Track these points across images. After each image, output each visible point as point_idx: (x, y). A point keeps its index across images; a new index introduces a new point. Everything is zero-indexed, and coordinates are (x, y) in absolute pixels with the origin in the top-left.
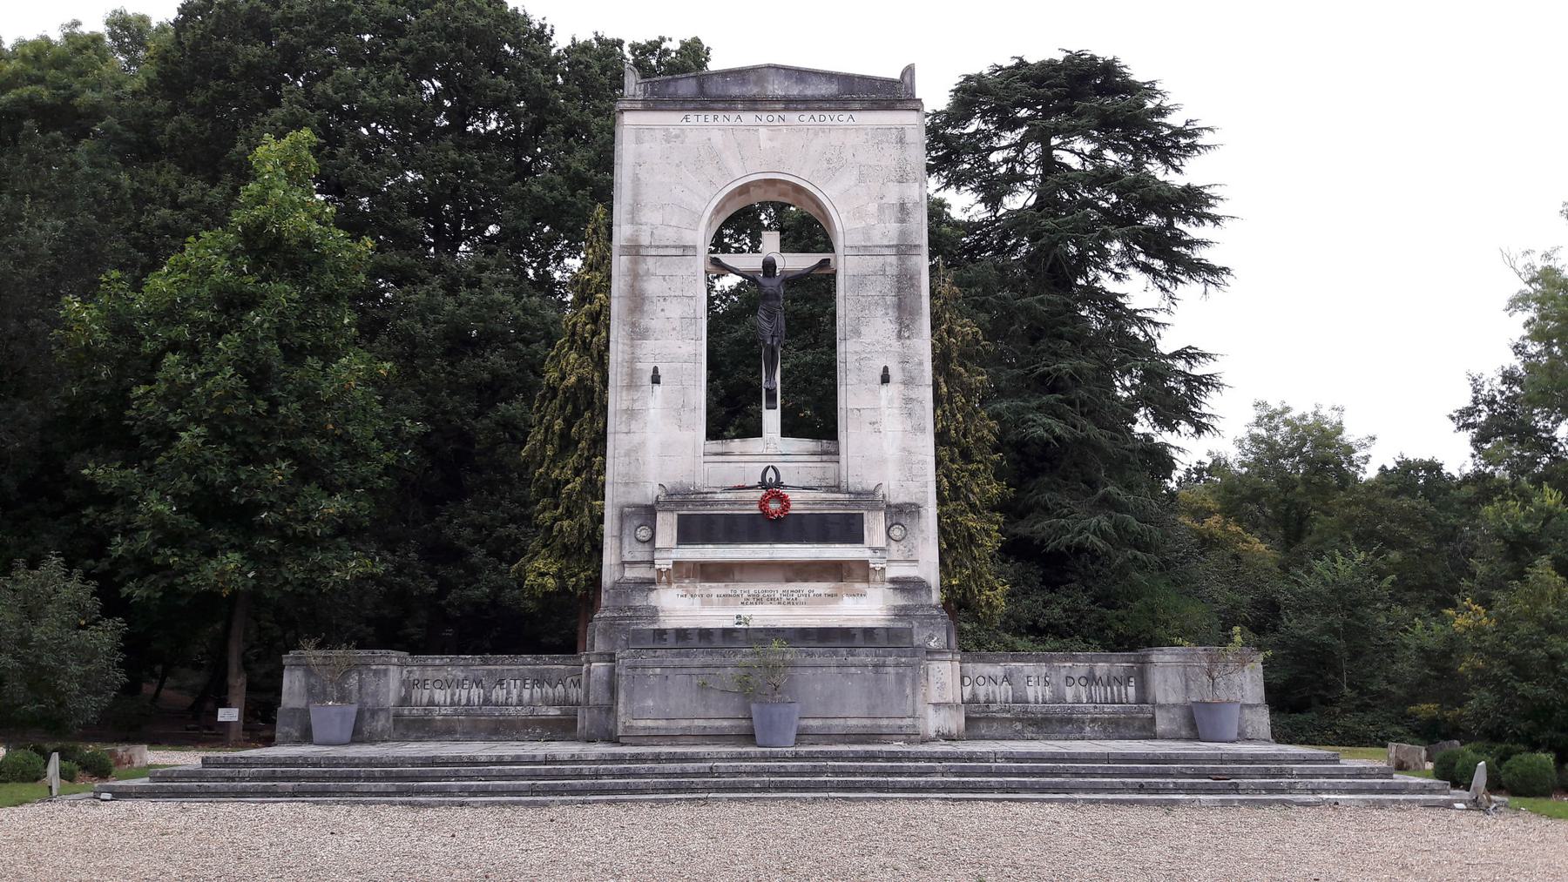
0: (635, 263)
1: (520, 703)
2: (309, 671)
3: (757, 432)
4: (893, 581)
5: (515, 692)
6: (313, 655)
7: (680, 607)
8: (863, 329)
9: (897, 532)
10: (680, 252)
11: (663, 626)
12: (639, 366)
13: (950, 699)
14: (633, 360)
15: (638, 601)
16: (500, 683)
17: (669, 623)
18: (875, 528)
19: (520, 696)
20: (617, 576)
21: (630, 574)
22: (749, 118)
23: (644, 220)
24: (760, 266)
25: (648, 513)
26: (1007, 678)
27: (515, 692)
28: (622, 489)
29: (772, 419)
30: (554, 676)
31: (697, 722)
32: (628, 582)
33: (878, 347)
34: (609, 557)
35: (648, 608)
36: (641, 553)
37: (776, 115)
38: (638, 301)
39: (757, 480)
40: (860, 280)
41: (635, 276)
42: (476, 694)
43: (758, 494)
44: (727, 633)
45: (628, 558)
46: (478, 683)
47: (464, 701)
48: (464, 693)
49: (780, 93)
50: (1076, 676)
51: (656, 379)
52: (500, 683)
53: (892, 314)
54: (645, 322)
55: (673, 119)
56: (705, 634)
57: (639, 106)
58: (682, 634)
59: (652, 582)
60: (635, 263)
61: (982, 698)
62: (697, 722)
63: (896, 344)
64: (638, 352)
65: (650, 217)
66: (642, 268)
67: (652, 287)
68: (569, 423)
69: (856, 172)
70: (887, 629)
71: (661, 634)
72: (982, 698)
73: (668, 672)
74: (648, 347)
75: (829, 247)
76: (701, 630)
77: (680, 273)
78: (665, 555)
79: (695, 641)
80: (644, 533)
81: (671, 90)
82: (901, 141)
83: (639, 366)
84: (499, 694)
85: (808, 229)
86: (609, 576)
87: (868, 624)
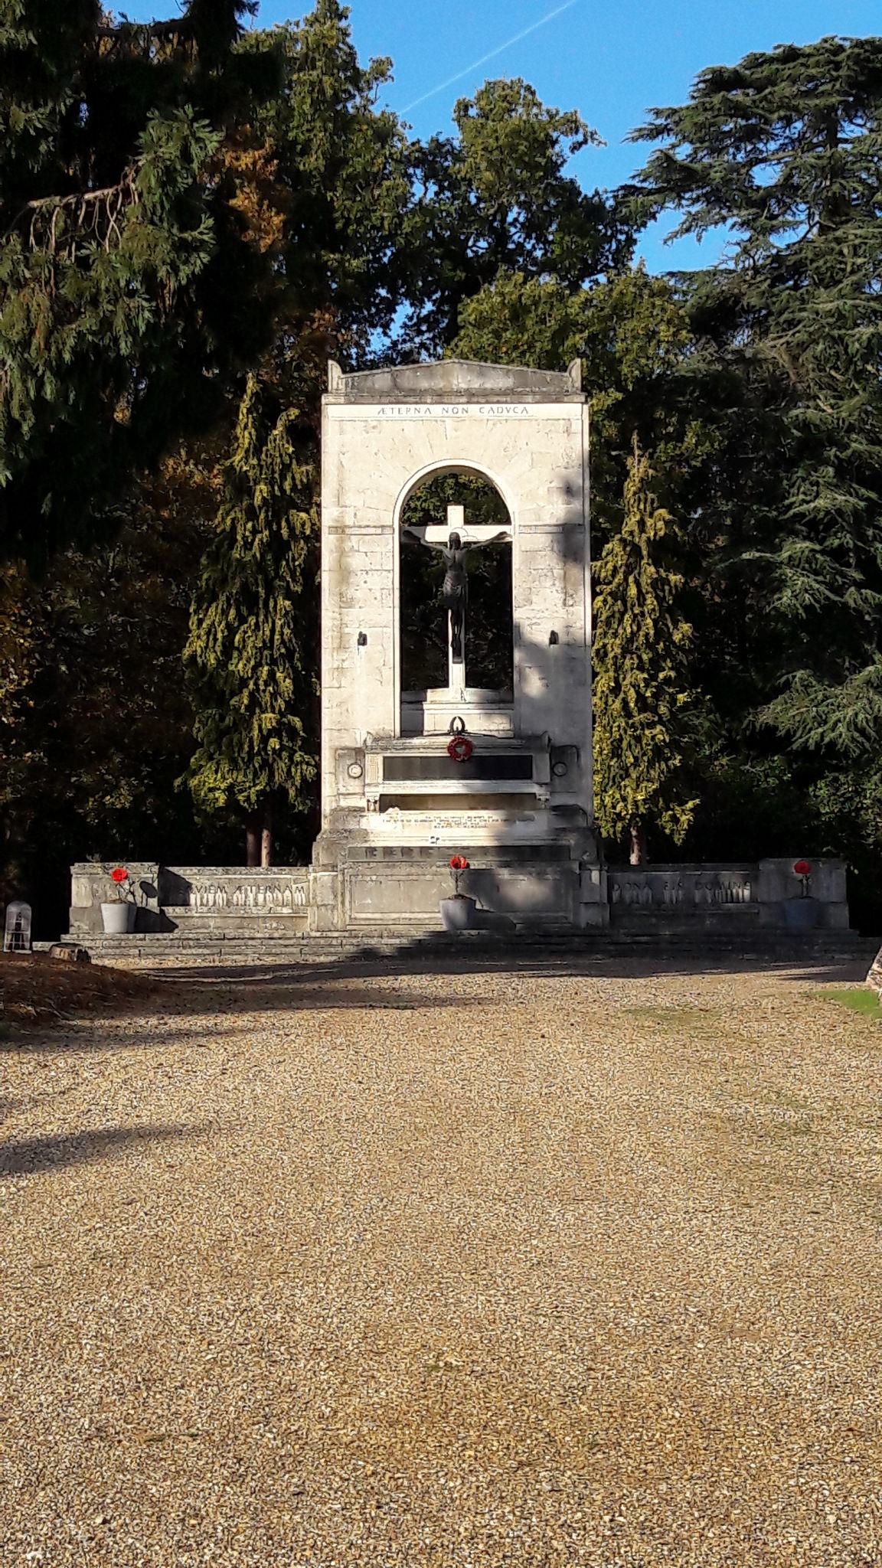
0: (342, 541)
1: (256, 904)
2: (92, 881)
3: (444, 683)
4: (555, 808)
5: (251, 896)
6: (96, 867)
7: (389, 830)
8: (534, 598)
9: (559, 769)
10: (379, 531)
11: (373, 845)
12: (346, 630)
13: (597, 899)
14: (342, 625)
15: (352, 825)
16: (239, 888)
17: (378, 843)
18: (542, 765)
19: (255, 899)
20: (334, 805)
21: (344, 803)
22: (437, 409)
23: (348, 503)
24: (446, 539)
25: (358, 754)
26: (649, 884)
27: (251, 896)
28: (336, 734)
29: (457, 671)
30: (283, 884)
31: (404, 915)
32: (343, 809)
33: (546, 614)
34: (327, 790)
35: (360, 830)
36: (355, 786)
37: (460, 407)
38: (344, 574)
39: (447, 728)
40: (531, 554)
41: (342, 553)
42: (221, 897)
43: (449, 739)
44: (424, 850)
45: (343, 790)
46: (222, 889)
47: (211, 903)
48: (211, 897)
49: (463, 386)
50: (703, 881)
51: (363, 640)
52: (239, 888)
53: (559, 585)
54: (350, 592)
55: (370, 411)
56: (407, 851)
57: (342, 400)
58: (388, 851)
59: (361, 810)
60: (342, 541)
61: (628, 900)
62: (404, 915)
63: (562, 612)
64: (346, 619)
65: (350, 499)
66: (348, 545)
67: (356, 562)
68: (231, 630)
69: (528, 458)
70: (551, 846)
71: (372, 851)
72: (628, 900)
73: (381, 879)
74: (353, 615)
75: (507, 521)
76: (403, 848)
77: (378, 549)
78: (373, 789)
79: (399, 857)
80: (356, 770)
81: (369, 384)
82: (568, 431)
83: (346, 630)
84: (238, 897)
85: (485, 502)
86: (327, 805)
87: (535, 843)
